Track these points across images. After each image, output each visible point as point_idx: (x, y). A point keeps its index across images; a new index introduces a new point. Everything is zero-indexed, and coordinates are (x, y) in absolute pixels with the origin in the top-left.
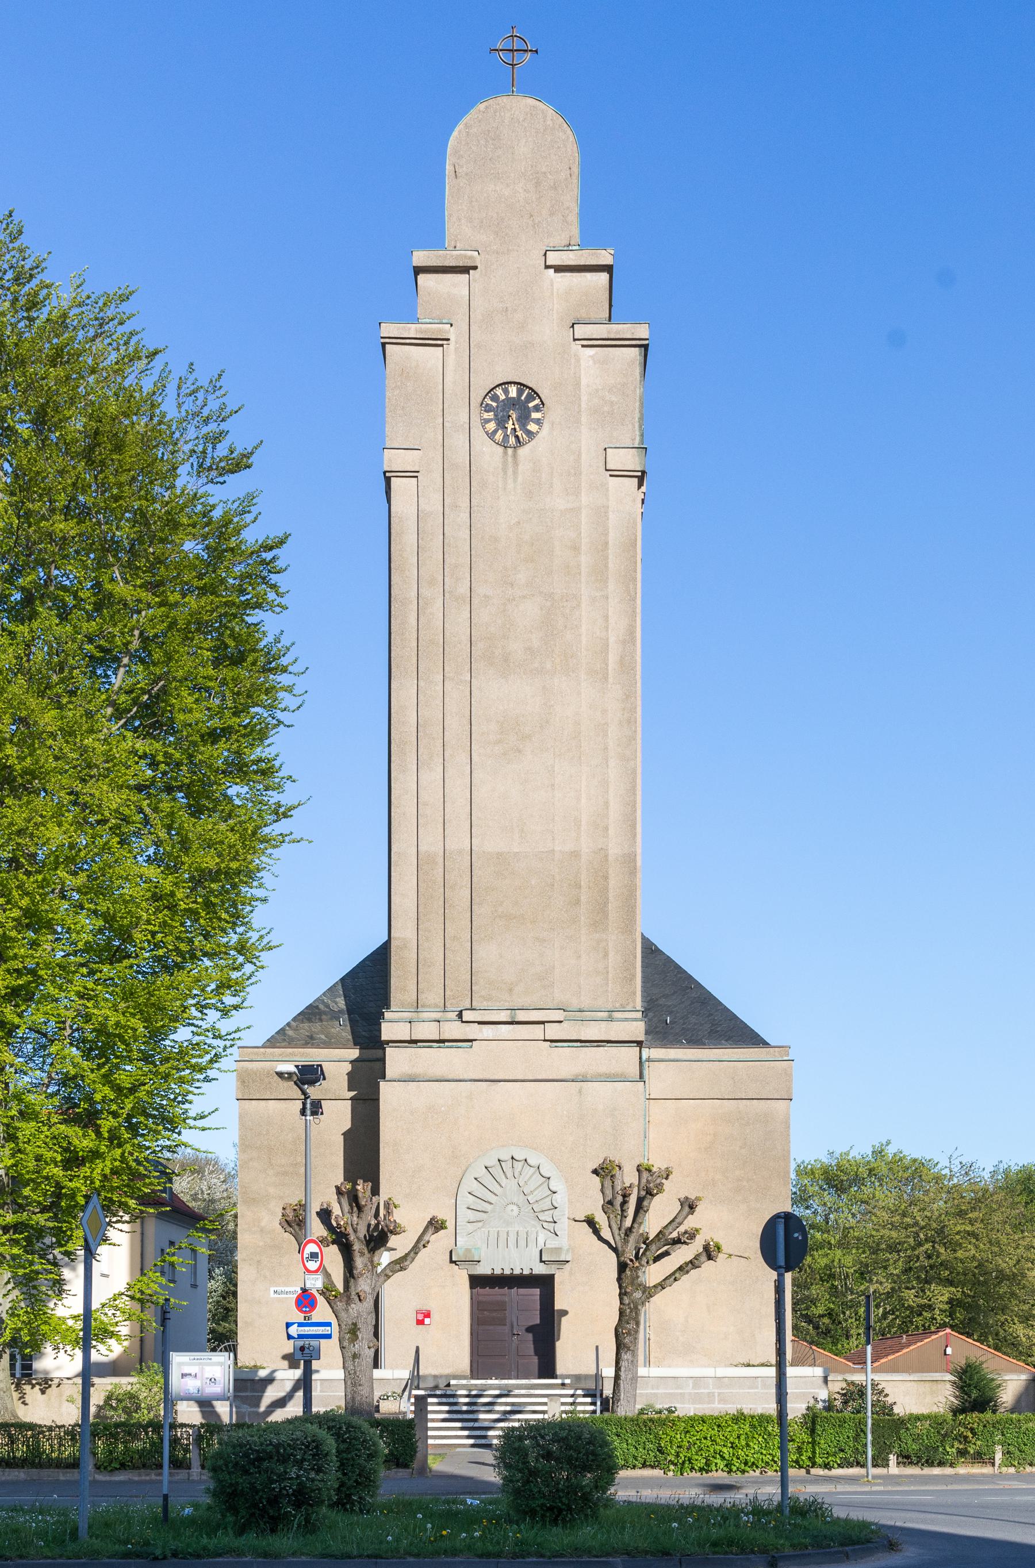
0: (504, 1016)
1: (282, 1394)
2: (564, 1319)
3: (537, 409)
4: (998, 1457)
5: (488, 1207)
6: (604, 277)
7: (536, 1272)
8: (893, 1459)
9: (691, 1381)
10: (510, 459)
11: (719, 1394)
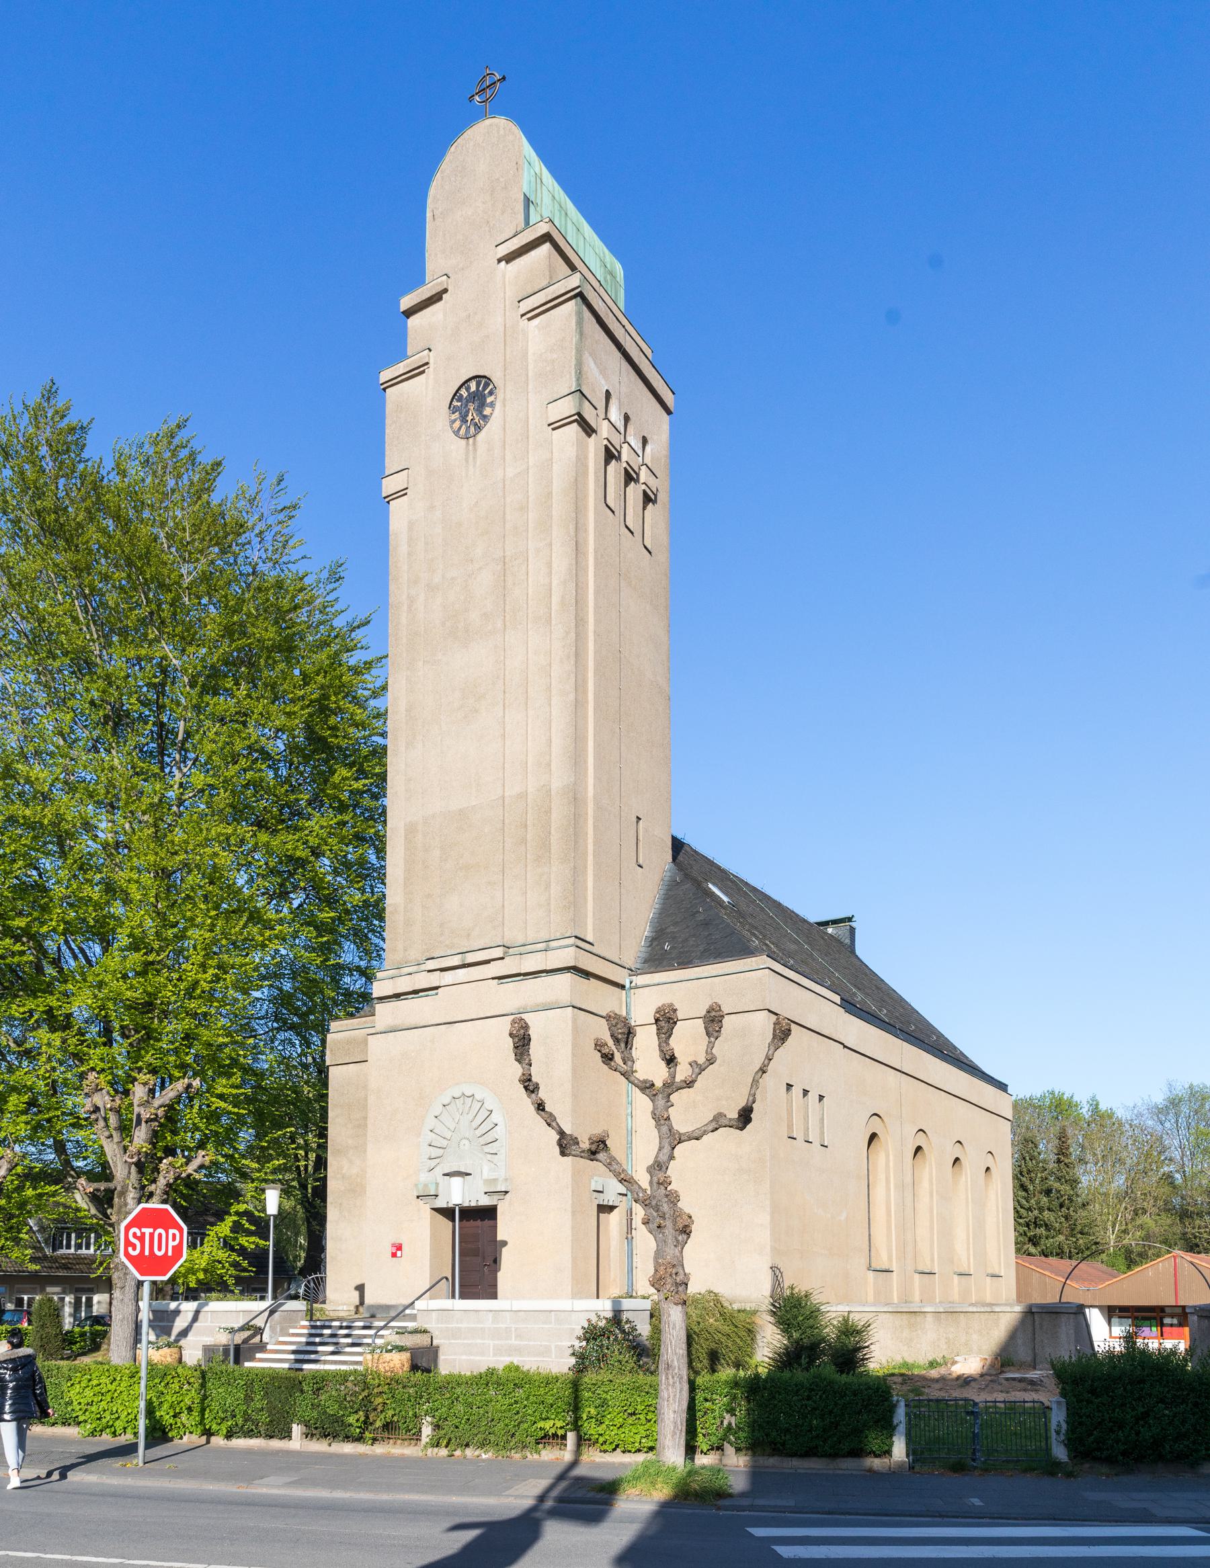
0: (456, 961)
1: (186, 1324)
2: (504, 1250)
3: (491, 393)
4: (427, 1431)
5: (483, 1140)
6: (546, 247)
7: (481, 1203)
8: (297, 1430)
9: (491, 1314)
10: (471, 448)
11: (516, 1329)
